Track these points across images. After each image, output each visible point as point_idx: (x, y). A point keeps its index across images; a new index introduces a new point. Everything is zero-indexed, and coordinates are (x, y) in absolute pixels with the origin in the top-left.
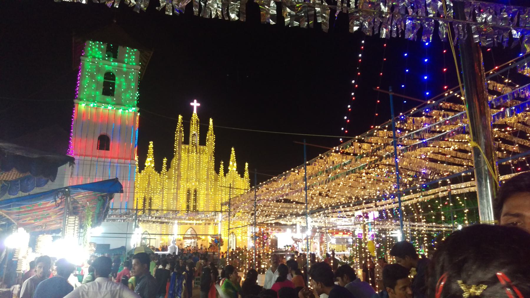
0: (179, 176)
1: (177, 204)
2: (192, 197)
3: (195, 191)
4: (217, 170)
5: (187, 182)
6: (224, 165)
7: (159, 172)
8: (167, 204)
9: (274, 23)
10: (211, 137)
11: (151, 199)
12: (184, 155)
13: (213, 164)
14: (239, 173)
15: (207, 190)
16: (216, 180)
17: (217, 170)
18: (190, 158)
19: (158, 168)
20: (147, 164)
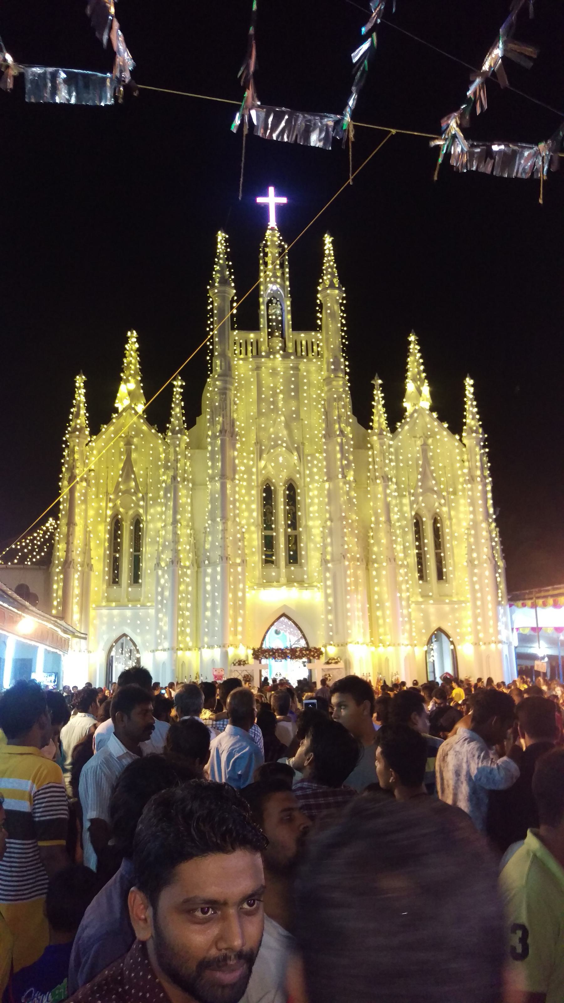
0: (229, 432)
1: (224, 530)
2: (281, 506)
3: (291, 488)
4: (363, 414)
6: (384, 388)
7: (162, 430)
10: (331, 295)
12: (242, 367)
13: (341, 384)
14: (441, 419)
16: (362, 444)
17: (363, 414)
18: (264, 373)
19: (157, 417)
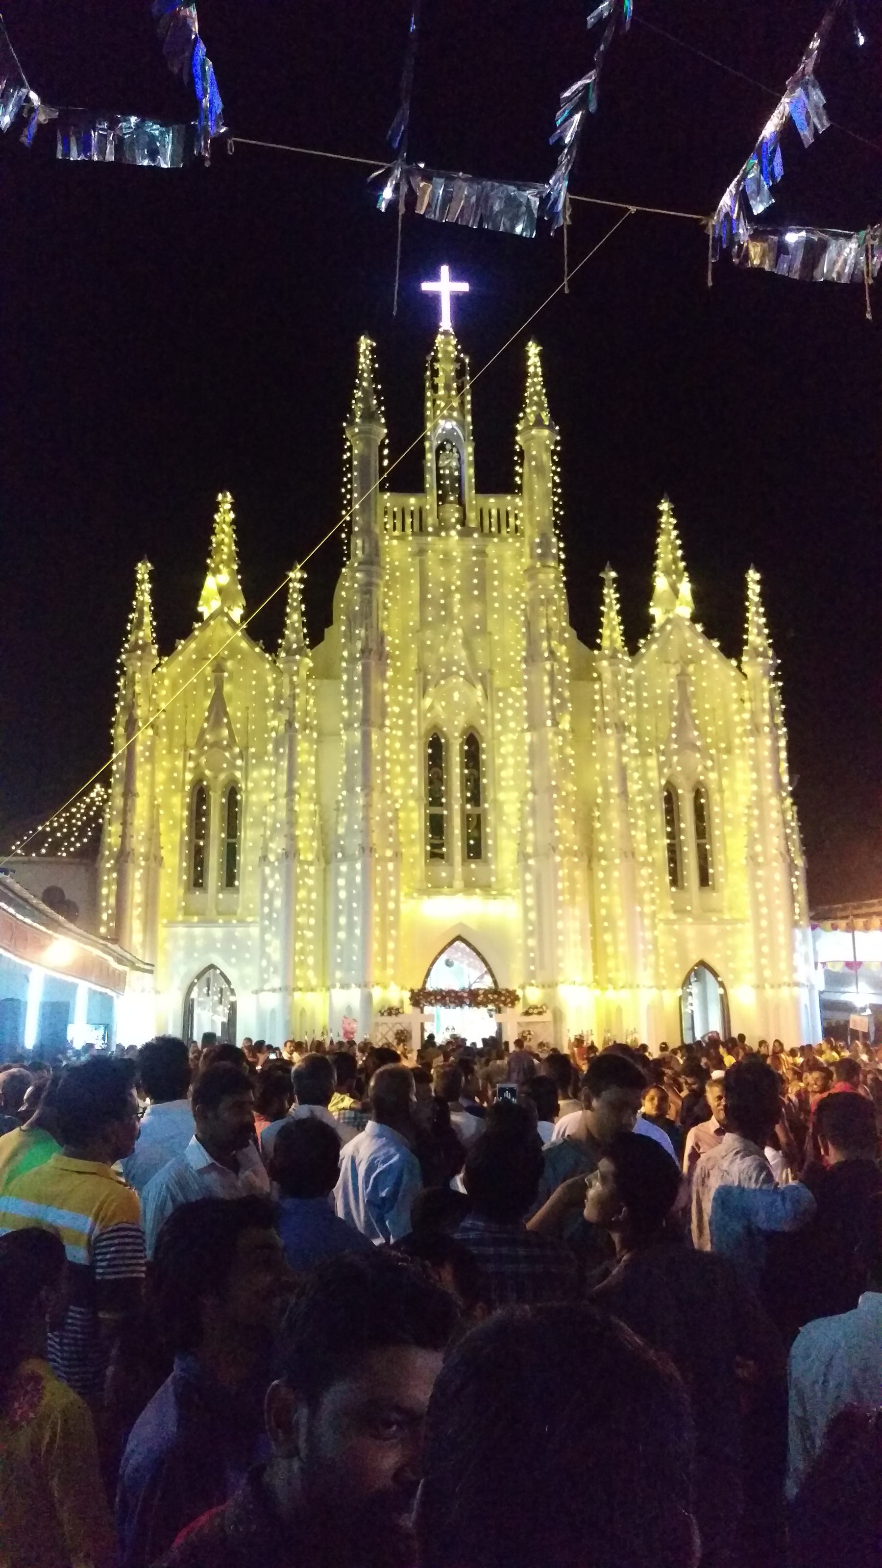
0: (375, 653)
1: (367, 806)
4: (585, 624)
5: (424, 693)
6: (620, 585)
7: (271, 648)
8: (322, 814)
9: (462, 1190)
10: (537, 438)
11: (232, 792)
12: (396, 549)
13: (553, 578)
14: (709, 634)
15: (534, 725)
16: (583, 673)
19: (265, 630)
20: (209, 602)
